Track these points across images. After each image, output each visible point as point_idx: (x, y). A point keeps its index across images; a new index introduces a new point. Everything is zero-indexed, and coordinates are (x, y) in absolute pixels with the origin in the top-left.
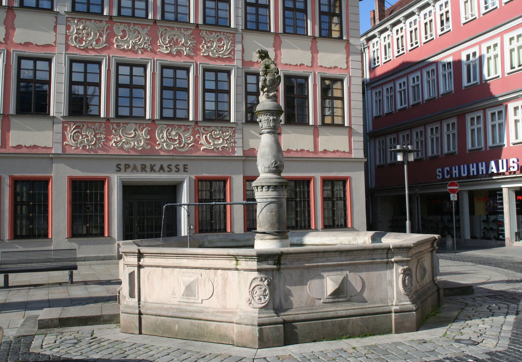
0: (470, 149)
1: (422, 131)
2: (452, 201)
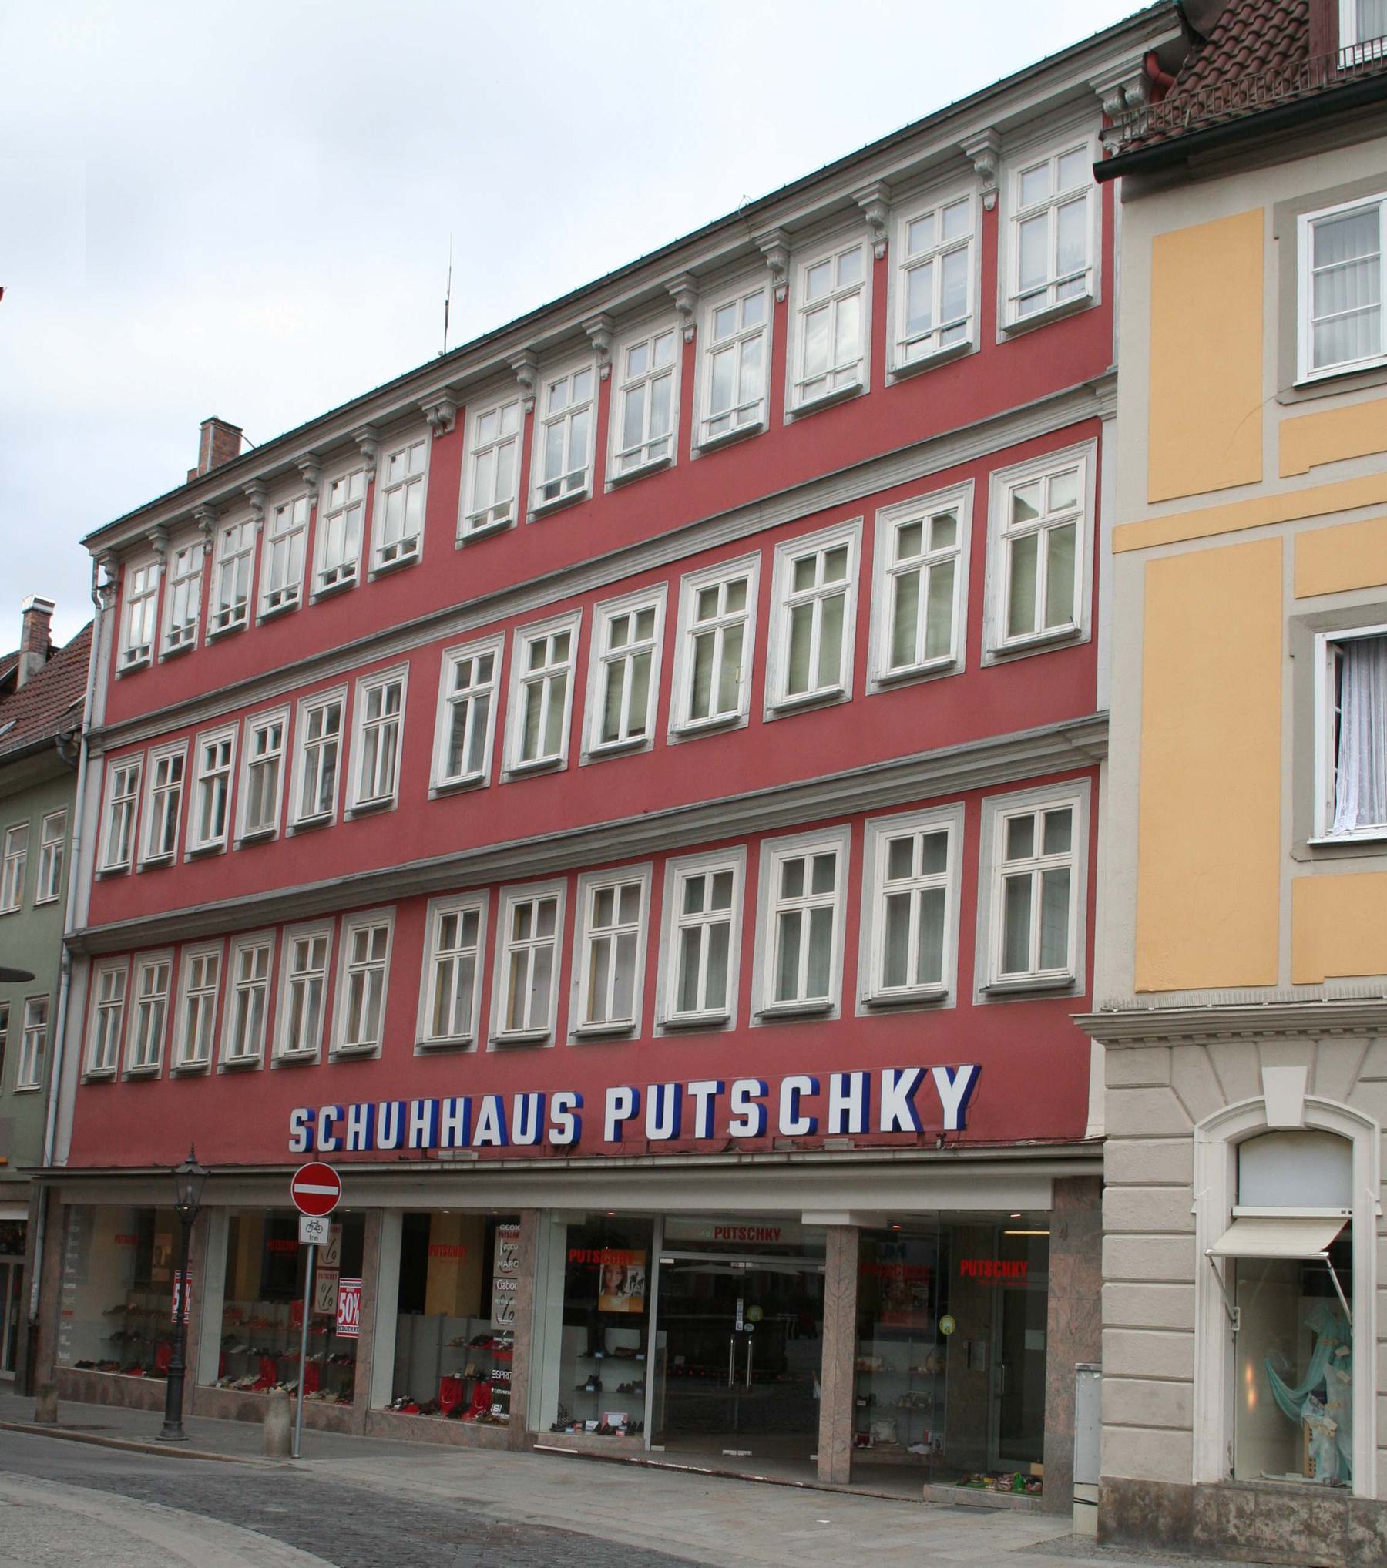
0: (425, 1040)
1: (166, 967)
2: (305, 1247)
